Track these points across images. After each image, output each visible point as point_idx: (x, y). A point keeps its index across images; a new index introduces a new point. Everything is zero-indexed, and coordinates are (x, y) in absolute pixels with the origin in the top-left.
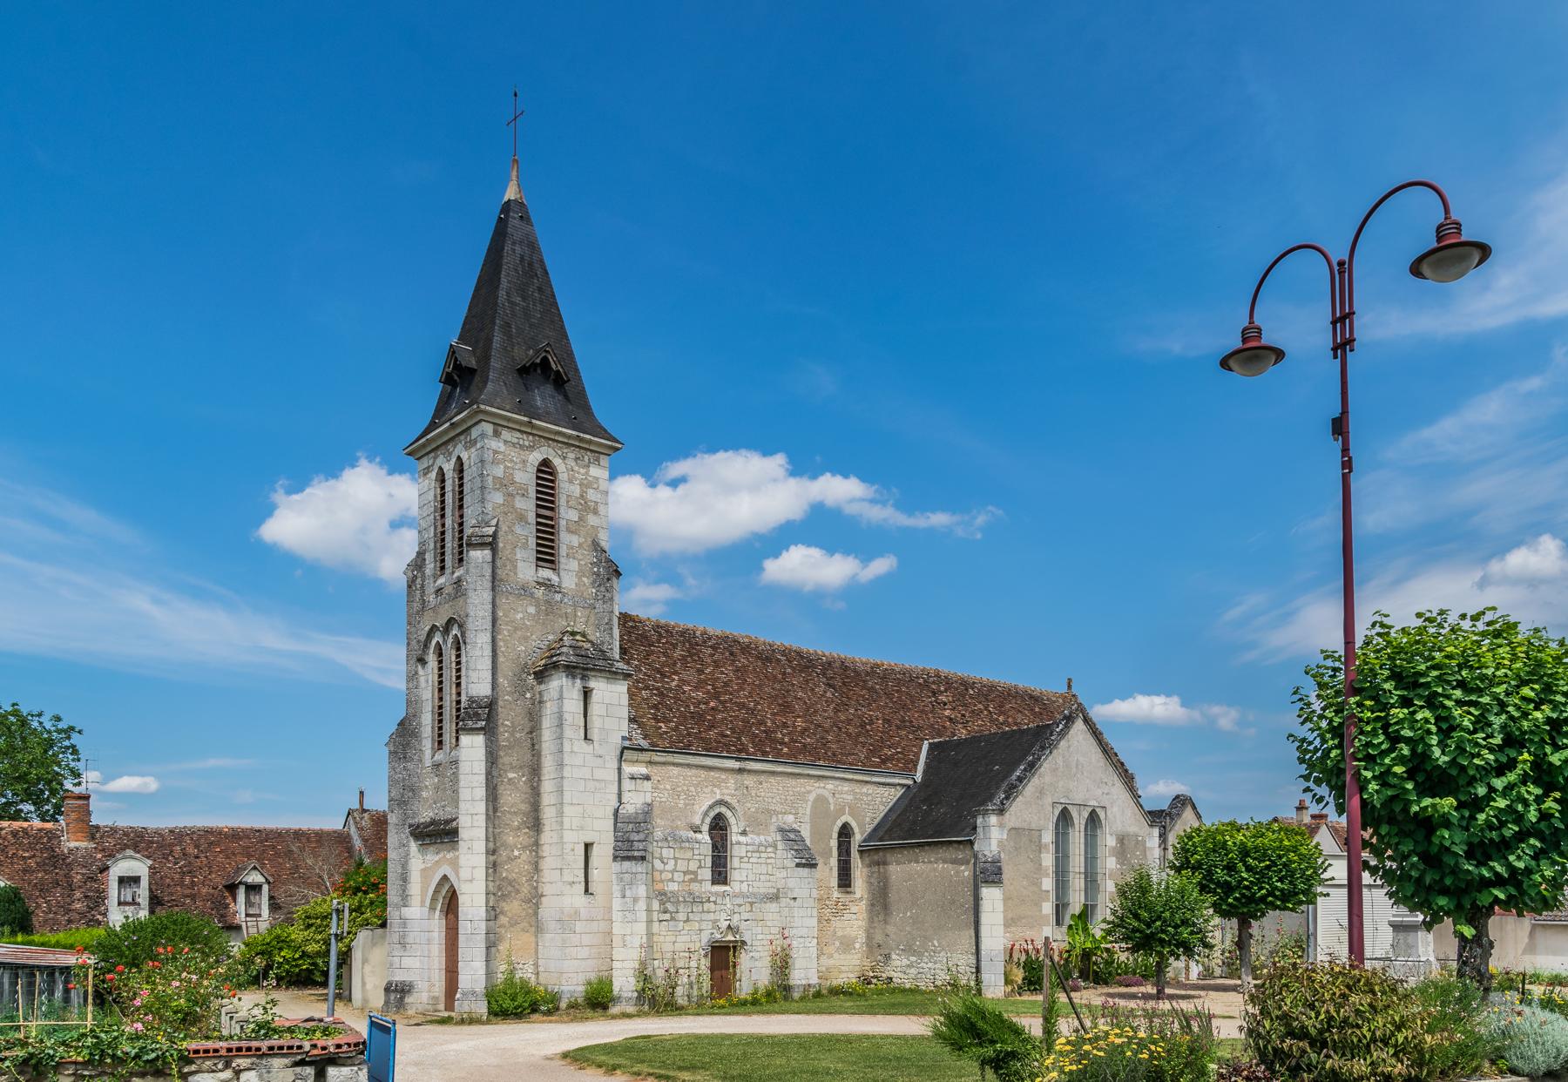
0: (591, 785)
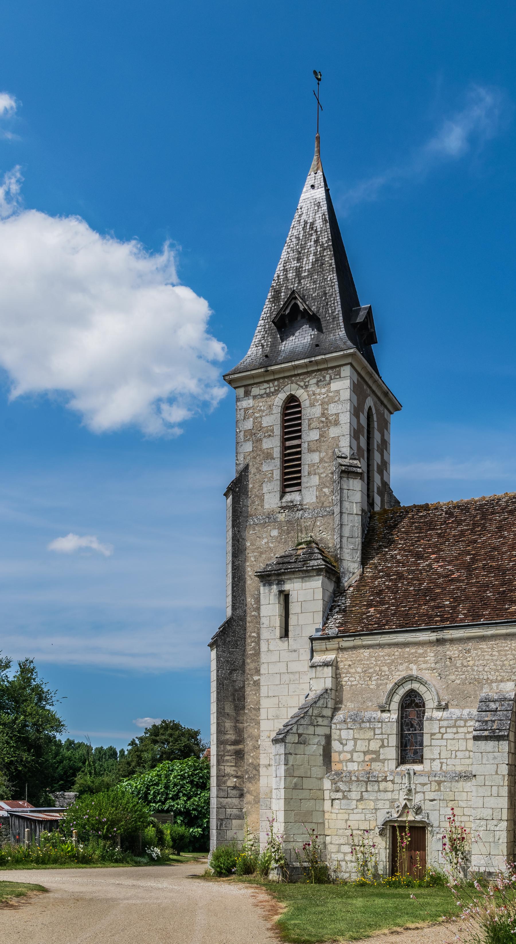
0: (286, 677)
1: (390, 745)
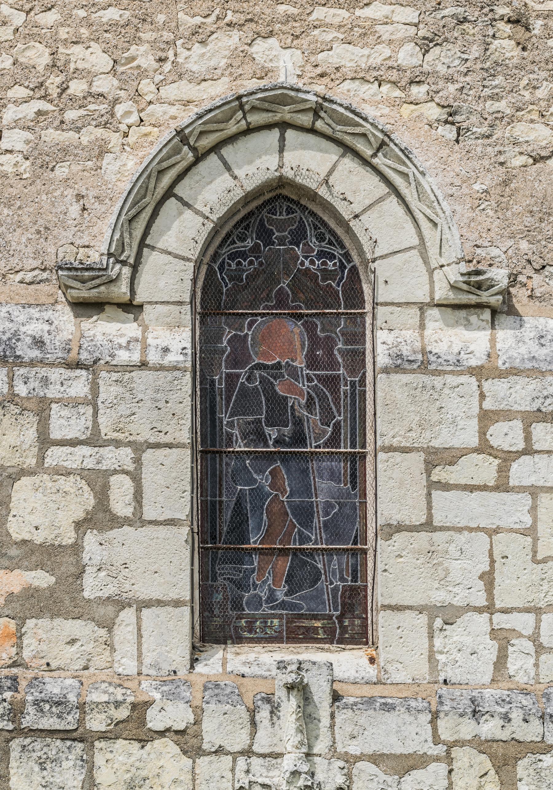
1: (149, 513)
